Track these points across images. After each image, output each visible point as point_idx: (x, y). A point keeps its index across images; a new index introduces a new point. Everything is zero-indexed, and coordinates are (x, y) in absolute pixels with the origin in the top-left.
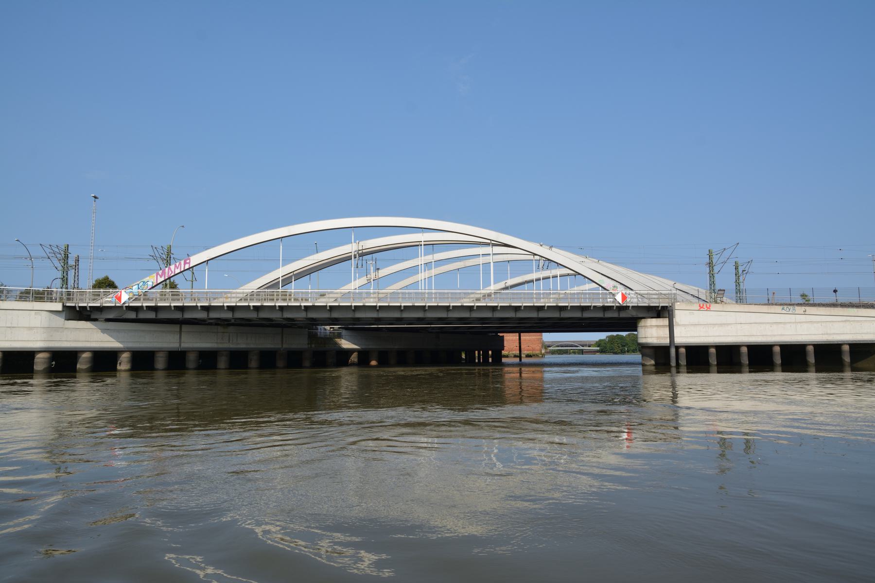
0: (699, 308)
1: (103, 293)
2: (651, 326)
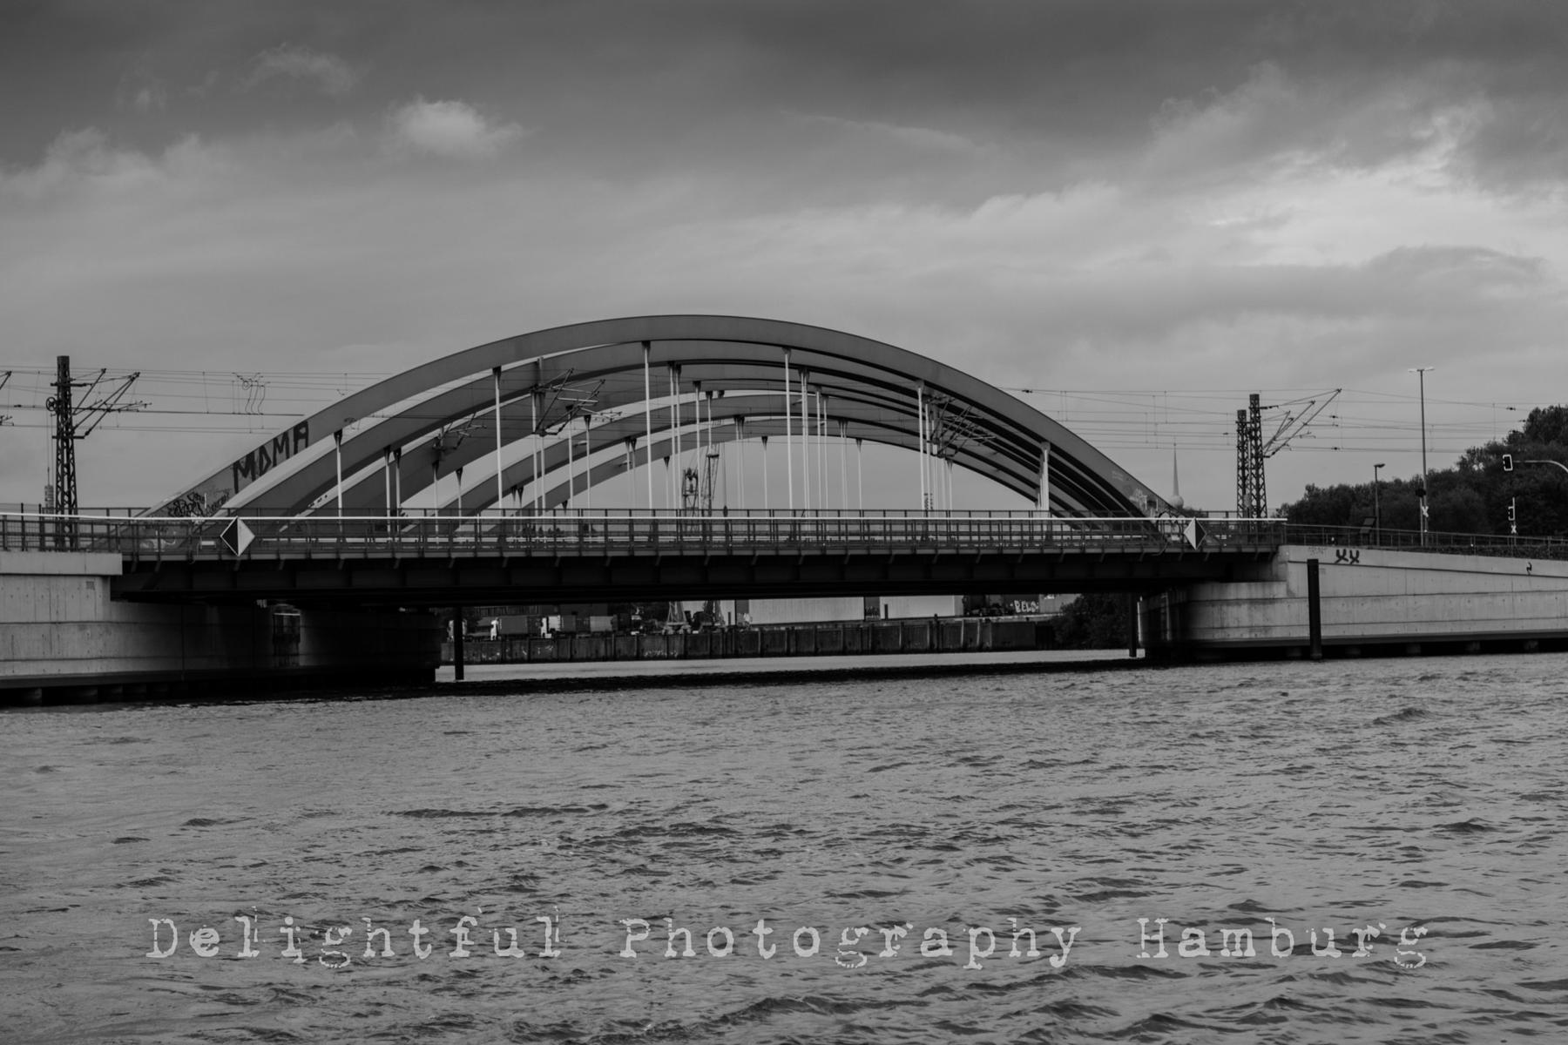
0: (1337, 559)
1: (941, 942)
2: (1238, 602)
